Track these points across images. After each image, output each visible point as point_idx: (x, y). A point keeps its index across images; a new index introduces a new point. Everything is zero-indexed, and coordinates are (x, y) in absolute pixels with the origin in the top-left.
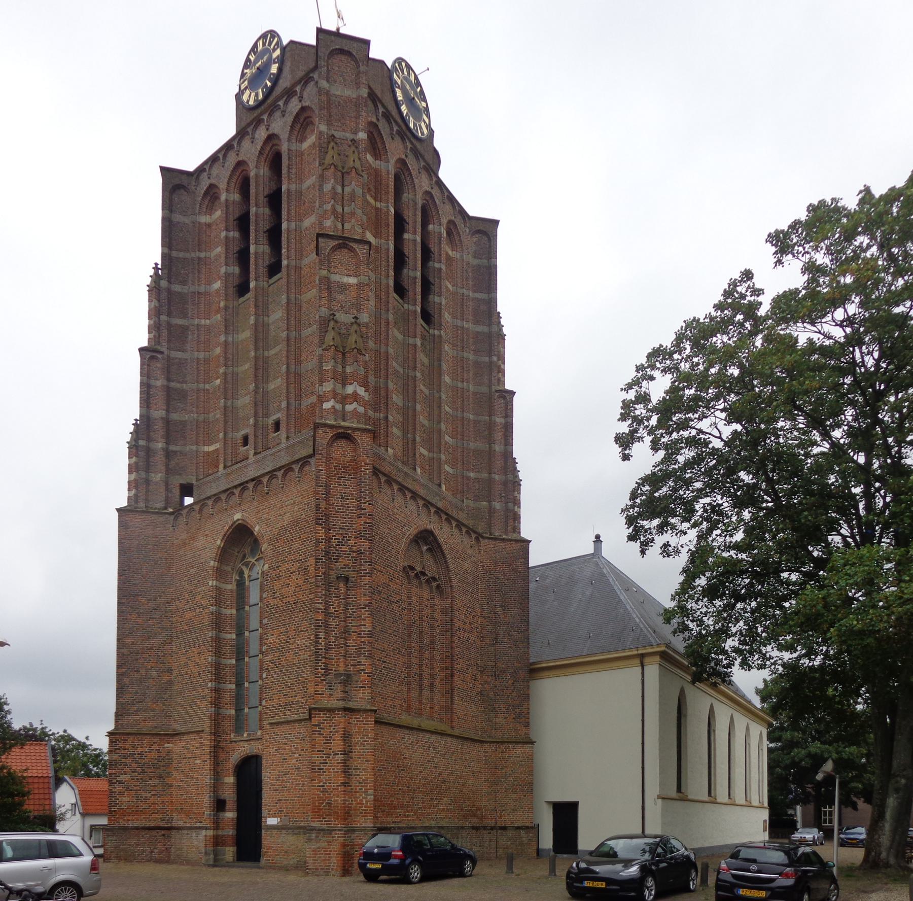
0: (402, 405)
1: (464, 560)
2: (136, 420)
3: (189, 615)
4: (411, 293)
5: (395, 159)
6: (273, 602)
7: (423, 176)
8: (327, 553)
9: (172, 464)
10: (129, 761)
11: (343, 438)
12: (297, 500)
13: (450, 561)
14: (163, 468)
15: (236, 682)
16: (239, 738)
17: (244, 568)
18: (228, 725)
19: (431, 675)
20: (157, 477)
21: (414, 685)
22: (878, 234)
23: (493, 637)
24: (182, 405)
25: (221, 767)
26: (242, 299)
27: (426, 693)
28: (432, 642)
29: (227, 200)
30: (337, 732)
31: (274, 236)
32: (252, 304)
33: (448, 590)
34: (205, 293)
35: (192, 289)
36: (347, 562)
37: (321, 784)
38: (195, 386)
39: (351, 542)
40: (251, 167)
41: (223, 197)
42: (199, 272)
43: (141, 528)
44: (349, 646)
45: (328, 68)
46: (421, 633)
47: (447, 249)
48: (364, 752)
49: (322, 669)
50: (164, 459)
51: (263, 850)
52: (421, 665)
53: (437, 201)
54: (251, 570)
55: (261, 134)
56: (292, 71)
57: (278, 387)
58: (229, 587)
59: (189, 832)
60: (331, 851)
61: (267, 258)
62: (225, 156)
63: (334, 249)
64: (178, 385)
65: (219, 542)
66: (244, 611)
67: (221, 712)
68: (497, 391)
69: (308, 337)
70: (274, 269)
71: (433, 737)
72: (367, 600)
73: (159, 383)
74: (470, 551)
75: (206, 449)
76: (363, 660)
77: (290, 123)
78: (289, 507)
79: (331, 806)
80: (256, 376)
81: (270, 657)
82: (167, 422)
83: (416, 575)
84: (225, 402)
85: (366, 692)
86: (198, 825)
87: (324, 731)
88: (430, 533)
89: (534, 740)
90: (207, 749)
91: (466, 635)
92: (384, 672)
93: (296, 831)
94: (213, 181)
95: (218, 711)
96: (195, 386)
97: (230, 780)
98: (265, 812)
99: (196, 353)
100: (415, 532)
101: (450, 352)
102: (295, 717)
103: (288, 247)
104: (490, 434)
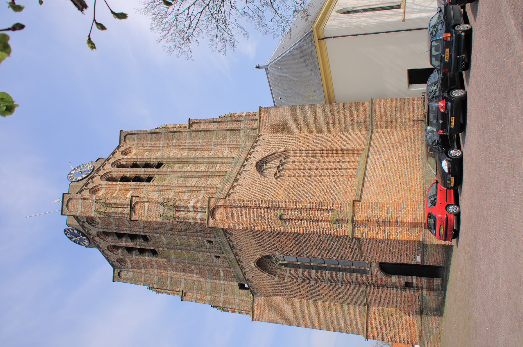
0: (197, 178)
1: (270, 144)
2: (211, 306)
4: (150, 173)
5: (101, 181)
6: (295, 252)
7: (106, 167)
11: (213, 214)
12: (243, 236)
13: (272, 152)
17: (278, 263)
19: (333, 163)
21: (340, 172)
22: (99, 221)
25: (386, 283)
26: (158, 252)
27: (344, 166)
28: (315, 162)
29: (122, 256)
31: (133, 237)
32: (159, 249)
33: (287, 153)
36: (273, 214)
37: (397, 234)
40: (109, 244)
41: (121, 257)
46: (310, 169)
47: (131, 155)
51: (436, 265)
52: (328, 169)
53: (115, 160)
54: (279, 260)
55: (97, 239)
57: (193, 240)
58: (288, 271)
62: (106, 255)
65: (266, 275)
66: (300, 264)
68: (189, 128)
70: (145, 238)
74: (266, 140)
77: (93, 227)
78: (247, 240)
83: (279, 171)
87: (366, 231)
88: (257, 164)
90: (376, 290)
91: (310, 142)
92: (332, 192)
94: (116, 260)
95: (354, 282)
97: (394, 279)
98: (413, 263)
101: (173, 152)
103: (136, 231)
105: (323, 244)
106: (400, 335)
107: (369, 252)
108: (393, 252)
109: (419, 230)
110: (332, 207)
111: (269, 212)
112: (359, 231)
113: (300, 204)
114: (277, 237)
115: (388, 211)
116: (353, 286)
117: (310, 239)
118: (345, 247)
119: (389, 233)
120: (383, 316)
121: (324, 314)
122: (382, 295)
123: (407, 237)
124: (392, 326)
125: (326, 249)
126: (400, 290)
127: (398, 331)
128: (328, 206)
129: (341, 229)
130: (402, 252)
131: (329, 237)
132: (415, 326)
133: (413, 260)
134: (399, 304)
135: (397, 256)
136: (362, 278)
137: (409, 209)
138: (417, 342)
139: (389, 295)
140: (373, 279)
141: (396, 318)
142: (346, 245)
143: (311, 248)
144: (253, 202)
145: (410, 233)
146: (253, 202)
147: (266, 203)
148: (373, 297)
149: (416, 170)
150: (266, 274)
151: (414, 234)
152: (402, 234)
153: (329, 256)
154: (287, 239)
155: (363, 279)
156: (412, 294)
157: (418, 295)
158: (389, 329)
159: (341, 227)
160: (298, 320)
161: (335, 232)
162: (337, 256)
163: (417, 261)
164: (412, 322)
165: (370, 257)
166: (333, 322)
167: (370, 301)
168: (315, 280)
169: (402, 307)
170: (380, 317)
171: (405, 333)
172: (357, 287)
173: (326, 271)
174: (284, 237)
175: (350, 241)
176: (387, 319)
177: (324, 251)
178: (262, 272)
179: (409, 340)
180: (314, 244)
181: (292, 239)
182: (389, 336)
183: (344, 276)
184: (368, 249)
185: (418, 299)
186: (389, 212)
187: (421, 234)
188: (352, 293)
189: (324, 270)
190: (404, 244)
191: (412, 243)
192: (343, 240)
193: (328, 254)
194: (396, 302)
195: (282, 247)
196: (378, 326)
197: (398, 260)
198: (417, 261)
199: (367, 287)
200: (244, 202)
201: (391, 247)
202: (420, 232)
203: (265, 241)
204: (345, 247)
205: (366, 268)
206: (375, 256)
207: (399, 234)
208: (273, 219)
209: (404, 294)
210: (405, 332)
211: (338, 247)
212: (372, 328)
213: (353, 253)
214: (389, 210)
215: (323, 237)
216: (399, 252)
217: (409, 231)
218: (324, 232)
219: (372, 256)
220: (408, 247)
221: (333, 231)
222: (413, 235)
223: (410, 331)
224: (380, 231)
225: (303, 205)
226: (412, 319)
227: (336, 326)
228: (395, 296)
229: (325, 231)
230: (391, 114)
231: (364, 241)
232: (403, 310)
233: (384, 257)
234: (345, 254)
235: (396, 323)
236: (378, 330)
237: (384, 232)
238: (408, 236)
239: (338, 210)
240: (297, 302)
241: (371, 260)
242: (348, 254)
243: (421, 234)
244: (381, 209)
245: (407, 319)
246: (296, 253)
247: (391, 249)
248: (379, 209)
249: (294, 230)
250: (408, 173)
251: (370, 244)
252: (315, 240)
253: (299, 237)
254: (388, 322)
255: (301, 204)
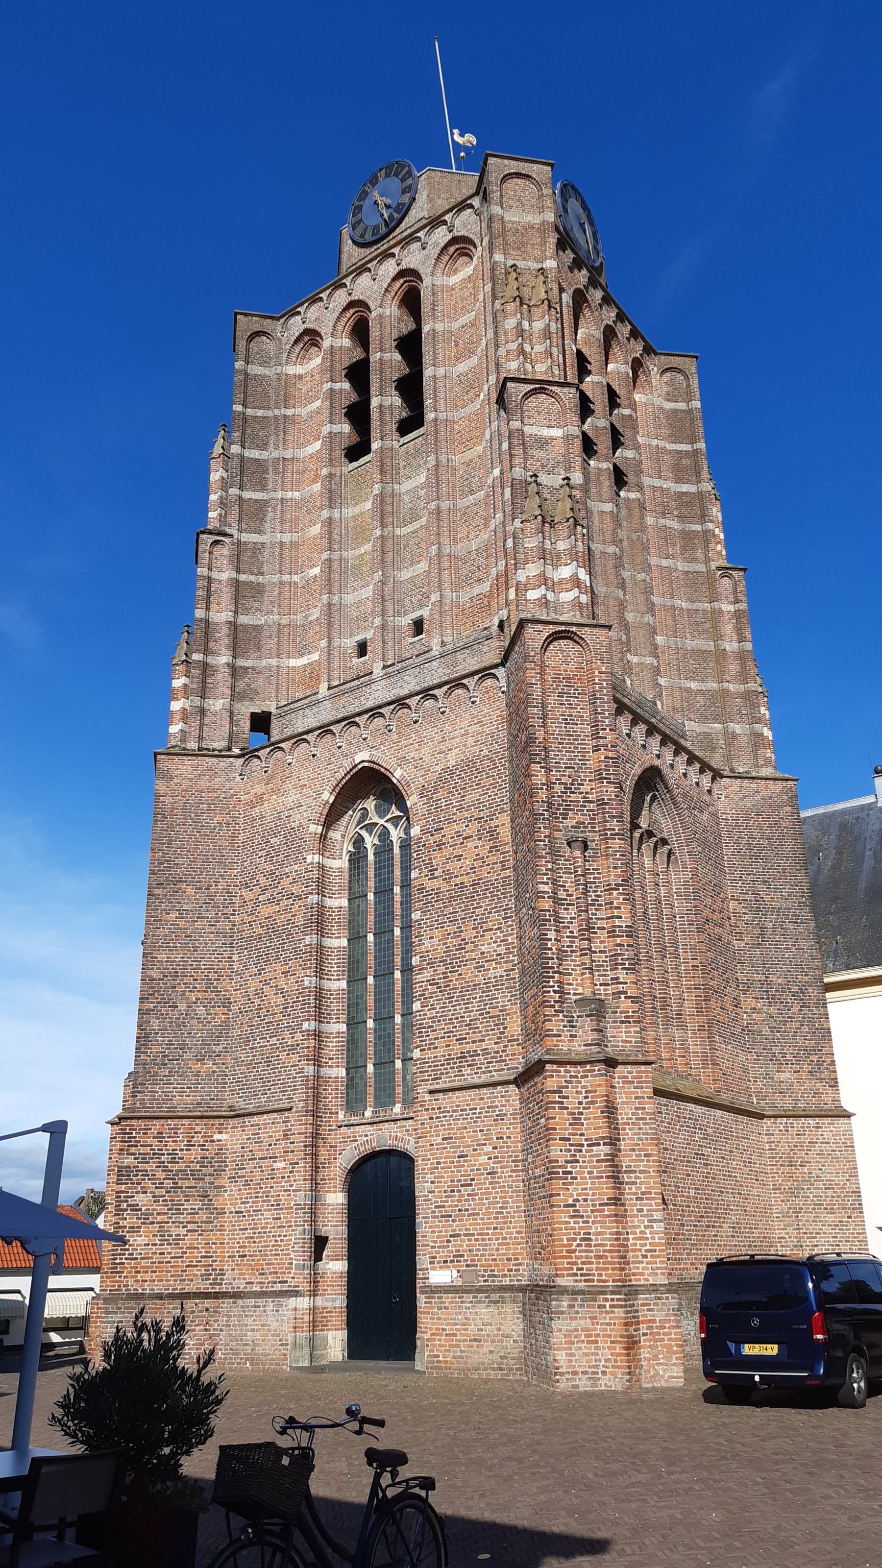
3: (266, 910)
5: (572, 290)
8: (550, 805)
9: (241, 685)
10: (151, 1167)
12: (471, 730)
14: (229, 691)
15: (348, 1019)
16: (354, 1120)
17: (364, 833)
18: (334, 1097)
20: (217, 705)
23: (757, 931)
24: (255, 605)
26: (355, 464)
30: (592, 1102)
34: (293, 459)
35: (275, 454)
37: (570, 1202)
38: (276, 578)
39: (585, 788)
42: (285, 433)
43: (191, 780)
44: (595, 952)
45: (501, 192)
48: (640, 1139)
49: (555, 992)
50: (229, 678)
56: (430, 199)
58: (336, 864)
59: (260, 1302)
60: (598, 1335)
61: (396, 412)
63: (527, 395)
64: (252, 578)
67: (322, 1074)
69: (468, 507)
71: (698, 1109)
72: (619, 876)
73: (224, 576)
75: (293, 662)
76: (622, 975)
78: (458, 740)
79: (590, 1245)
80: (383, 561)
81: (427, 975)
82: (234, 626)
84: (329, 597)
85: (632, 1030)
86: (278, 1287)
89: (850, 1109)
90: (299, 1141)
91: (718, 930)
93: (495, 1296)
96: (276, 578)
98: (422, 1260)
99: (279, 535)
100: (639, 772)
102: (484, 1078)
104: (715, 628)
105: (468, 972)
106: (140, 1227)
107: (452, 1116)
108: (459, 1191)
109: (588, 1275)
110: (626, 998)
111: (585, 806)
112: (566, 1081)
113: (621, 900)
114: (479, 831)
115: (634, 1172)
116: (310, 1070)
117: (483, 931)
118: (465, 1038)
119: (569, 1176)
120: (201, 1170)
121: (194, 980)
122: (280, 1161)
123: (565, 1238)
124: (170, 1201)
125: (451, 981)
126: (304, 1221)
127: (152, 1223)
128: (626, 983)
129: (564, 1026)
130: (460, 1221)
131: (498, 990)
132: (171, 1276)
133: (435, 1257)
134: (246, 1220)
135: (444, 1207)
136: (334, 1097)
137: (647, 1239)
138: (119, 1286)
139: (283, 1186)
140: (330, 1130)
141: (198, 1213)
142: (474, 1042)
143: (448, 934)
144: (611, 758)
145: (578, 1245)
146: (611, 758)
147: (613, 797)
148: (267, 1133)
149: (696, 1259)
150: (328, 797)
151: (574, 1260)
152: (572, 1221)
153: (423, 990)
154: (474, 860)
155: (328, 1098)
156: (294, 1262)
157: (289, 1280)
158: (158, 1192)
159: (570, 1026)
160: (171, 895)
161: (553, 1006)
162: (424, 1015)
163: (432, 1272)
164: (187, 1266)
165: (431, 1118)
166: (169, 1007)
167: (252, 1125)
168: (320, 949)
169: (236, 1230)
170: (195, 1158)
171: (148, 1245)
172: (307, 1080)
173: (348, 982)
174: (484, 852)
175: (488, 1054)
176: (192, 1183)
177: (443, 973)
178: (337, 785)
179: (126, 1259)
180: (467, 943)
181: (477, 876)
182: (137, 1193)
183: (334, 1038)
184: (461, 1110)
185: (275, 1283)
186: (633, 1175)
187: (576, 1281)
188: (279, 1064)
189: (349, 976)
190: (495, 1228)
191: (501, 1252)
192: (490, 1033)
193: (430, 985)
194: (254, 1211)
195: (445, 844)
196: (168, 1154)
197: (429, 1209)
198: (432, 1272)
199: (306, 1111)
200: (608, 731)
201: (480, 1184)
202: (583, 1278)
203: (460, 794)
204: (465, 1038)
205: (370, 1106)
206: (438, 1136)
207: (571, 1209)
208: (566, 819)
209: (290, 1235)
210: (153, 1245)
211: (462, 1017)
212: (159, 1136)
213: (443, 1065)
214: (638, 1174)
215: (495, 968)
216: (460, 1210)
217: (584, 1243)
218: (549, 972)
219: (437, 1126)
220: (483, 1240)
221: (555, 1001)
222: (573, 1255)
223: (155, 1263)
224: (572, 1148)
225: (620, 908)
226: (197, 1266)
227: (158, 1018)
228: (277, 1205)
229: (553, 977)
230: (814, 1175)
231: (495, 1097)
232: (223, 1235)
233: (439, 1163)
234: (435, 1039)
235: (179, 1212)
236: (154, 1154)
237: (571, 1162)
238: (568, 1240)
239: (618, 1014)
240: (229, 893)
241: (422, 1124)
242: (436, 1048)
243: (576, 1281)
244: (639, 1150)
245: (195, 1248)
246: (423, 889)
247: (471, 1185)
248: (639, 1145)
249: (545, 880)
250: (687, 1230)
251: (485, 1117)
252: (483, 945)
253: (487, 897)
254: (181, 1188)
255: (622, 904)
